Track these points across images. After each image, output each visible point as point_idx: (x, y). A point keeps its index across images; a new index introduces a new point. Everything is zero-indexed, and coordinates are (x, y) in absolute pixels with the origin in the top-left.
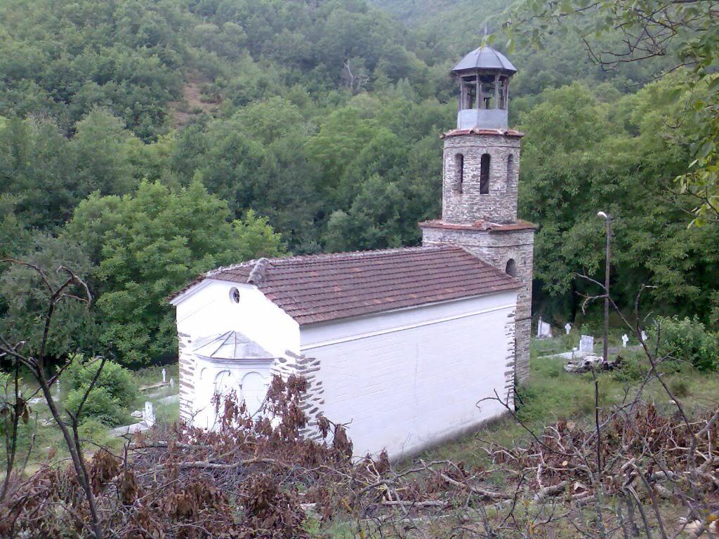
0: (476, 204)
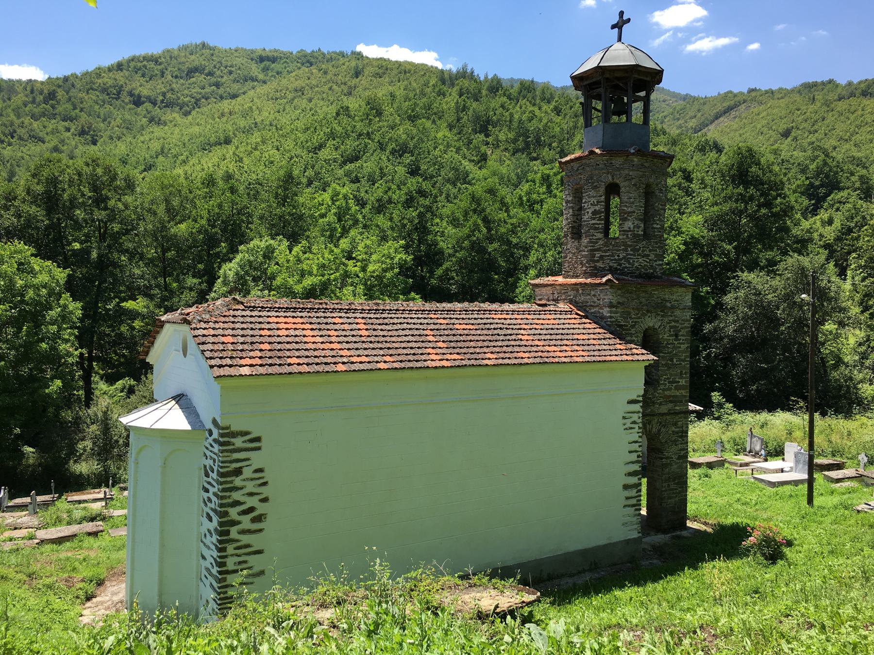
0: (598, 250)
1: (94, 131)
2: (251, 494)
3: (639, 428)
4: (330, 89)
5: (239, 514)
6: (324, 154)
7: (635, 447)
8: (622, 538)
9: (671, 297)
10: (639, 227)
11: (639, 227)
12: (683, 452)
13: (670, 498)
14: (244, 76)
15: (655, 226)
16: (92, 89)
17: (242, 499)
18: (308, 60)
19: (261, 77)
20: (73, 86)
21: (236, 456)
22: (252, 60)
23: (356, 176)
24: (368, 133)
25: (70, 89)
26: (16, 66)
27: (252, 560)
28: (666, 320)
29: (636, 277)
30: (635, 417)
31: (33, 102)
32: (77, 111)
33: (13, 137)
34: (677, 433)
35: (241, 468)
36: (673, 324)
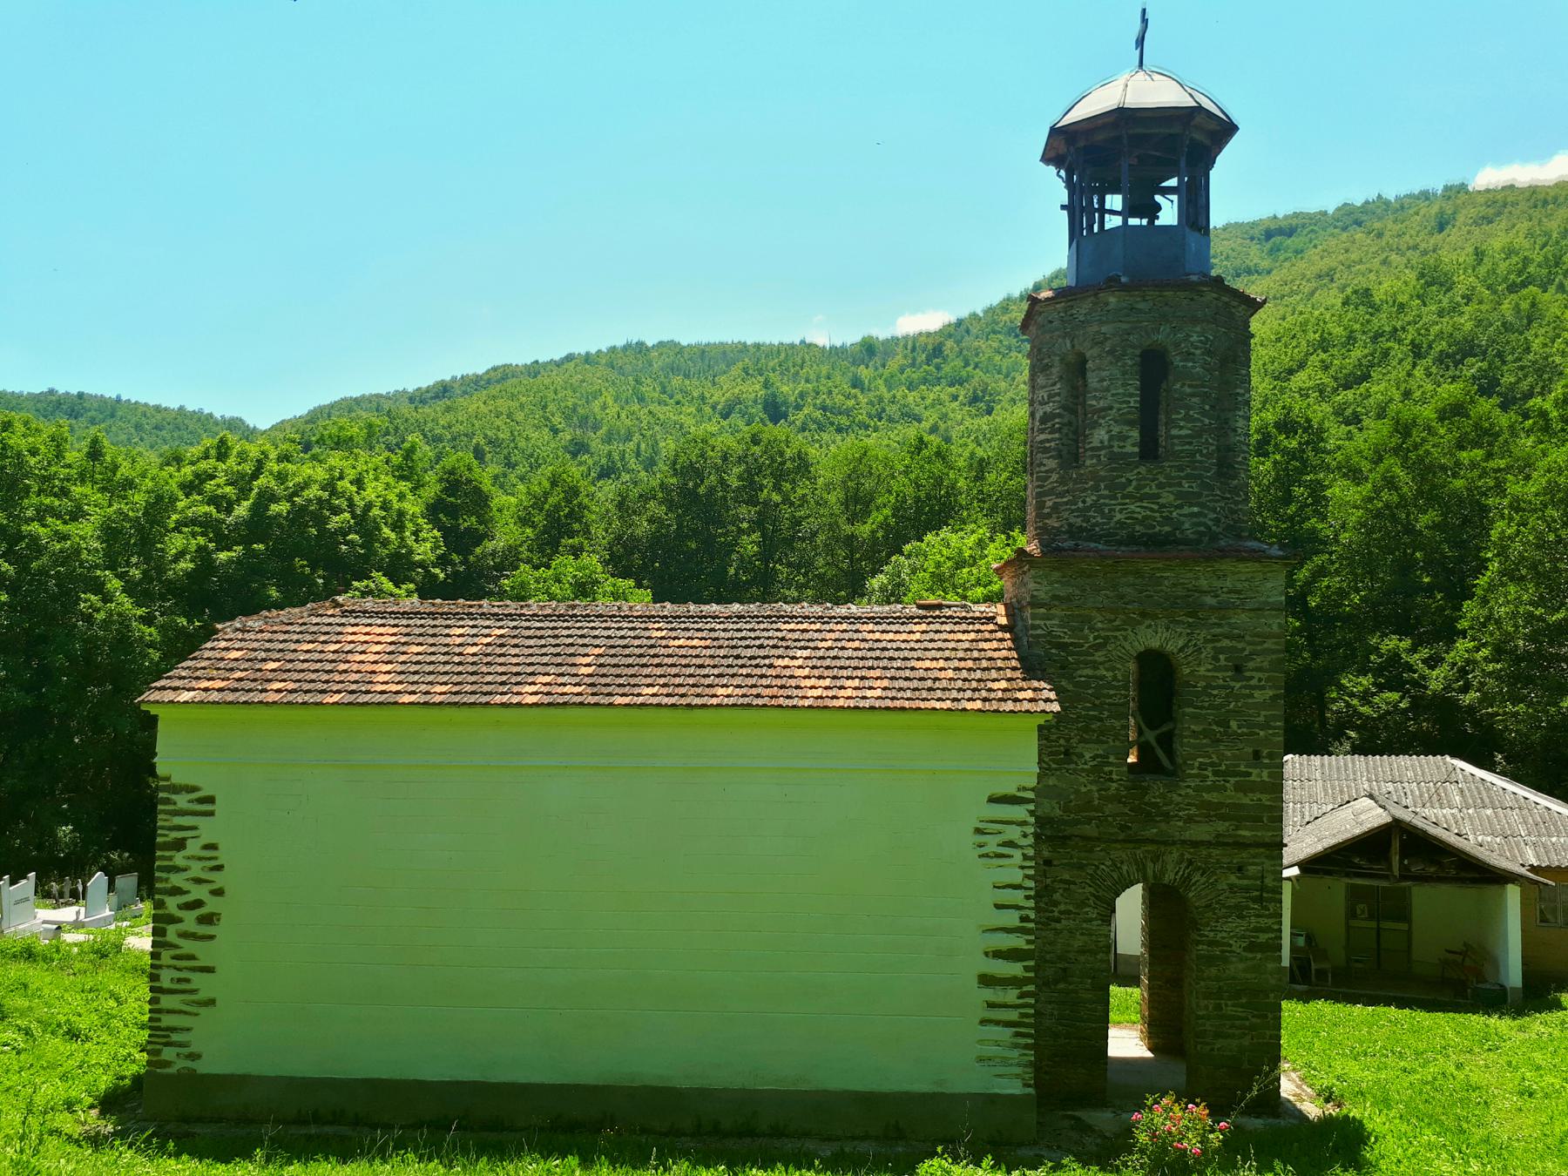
0: (1051, 492)
2: (198, 881)
4: (1385, 262)
5: (180, 907)
6: (1300, 379)
7: (1018, 897)
9: (1218, 584)
12: (1263, 937)
13: (1218, 1035)
15: (1174, 432)
16: (994, 332)
17: (185, 886)
18: (1351, 218)
19: (1265, 264)
20: (968, 331)
21: (178, 821)
22: (1252, 239)
23: (1355, 412)
24: (1396, 330)
27: (198, 980)
29: (1120, 543)
30: (1013, 833)
31: (913, 365)
34: (1247, 889)
35: (184, 839)
36: (1226, 643)
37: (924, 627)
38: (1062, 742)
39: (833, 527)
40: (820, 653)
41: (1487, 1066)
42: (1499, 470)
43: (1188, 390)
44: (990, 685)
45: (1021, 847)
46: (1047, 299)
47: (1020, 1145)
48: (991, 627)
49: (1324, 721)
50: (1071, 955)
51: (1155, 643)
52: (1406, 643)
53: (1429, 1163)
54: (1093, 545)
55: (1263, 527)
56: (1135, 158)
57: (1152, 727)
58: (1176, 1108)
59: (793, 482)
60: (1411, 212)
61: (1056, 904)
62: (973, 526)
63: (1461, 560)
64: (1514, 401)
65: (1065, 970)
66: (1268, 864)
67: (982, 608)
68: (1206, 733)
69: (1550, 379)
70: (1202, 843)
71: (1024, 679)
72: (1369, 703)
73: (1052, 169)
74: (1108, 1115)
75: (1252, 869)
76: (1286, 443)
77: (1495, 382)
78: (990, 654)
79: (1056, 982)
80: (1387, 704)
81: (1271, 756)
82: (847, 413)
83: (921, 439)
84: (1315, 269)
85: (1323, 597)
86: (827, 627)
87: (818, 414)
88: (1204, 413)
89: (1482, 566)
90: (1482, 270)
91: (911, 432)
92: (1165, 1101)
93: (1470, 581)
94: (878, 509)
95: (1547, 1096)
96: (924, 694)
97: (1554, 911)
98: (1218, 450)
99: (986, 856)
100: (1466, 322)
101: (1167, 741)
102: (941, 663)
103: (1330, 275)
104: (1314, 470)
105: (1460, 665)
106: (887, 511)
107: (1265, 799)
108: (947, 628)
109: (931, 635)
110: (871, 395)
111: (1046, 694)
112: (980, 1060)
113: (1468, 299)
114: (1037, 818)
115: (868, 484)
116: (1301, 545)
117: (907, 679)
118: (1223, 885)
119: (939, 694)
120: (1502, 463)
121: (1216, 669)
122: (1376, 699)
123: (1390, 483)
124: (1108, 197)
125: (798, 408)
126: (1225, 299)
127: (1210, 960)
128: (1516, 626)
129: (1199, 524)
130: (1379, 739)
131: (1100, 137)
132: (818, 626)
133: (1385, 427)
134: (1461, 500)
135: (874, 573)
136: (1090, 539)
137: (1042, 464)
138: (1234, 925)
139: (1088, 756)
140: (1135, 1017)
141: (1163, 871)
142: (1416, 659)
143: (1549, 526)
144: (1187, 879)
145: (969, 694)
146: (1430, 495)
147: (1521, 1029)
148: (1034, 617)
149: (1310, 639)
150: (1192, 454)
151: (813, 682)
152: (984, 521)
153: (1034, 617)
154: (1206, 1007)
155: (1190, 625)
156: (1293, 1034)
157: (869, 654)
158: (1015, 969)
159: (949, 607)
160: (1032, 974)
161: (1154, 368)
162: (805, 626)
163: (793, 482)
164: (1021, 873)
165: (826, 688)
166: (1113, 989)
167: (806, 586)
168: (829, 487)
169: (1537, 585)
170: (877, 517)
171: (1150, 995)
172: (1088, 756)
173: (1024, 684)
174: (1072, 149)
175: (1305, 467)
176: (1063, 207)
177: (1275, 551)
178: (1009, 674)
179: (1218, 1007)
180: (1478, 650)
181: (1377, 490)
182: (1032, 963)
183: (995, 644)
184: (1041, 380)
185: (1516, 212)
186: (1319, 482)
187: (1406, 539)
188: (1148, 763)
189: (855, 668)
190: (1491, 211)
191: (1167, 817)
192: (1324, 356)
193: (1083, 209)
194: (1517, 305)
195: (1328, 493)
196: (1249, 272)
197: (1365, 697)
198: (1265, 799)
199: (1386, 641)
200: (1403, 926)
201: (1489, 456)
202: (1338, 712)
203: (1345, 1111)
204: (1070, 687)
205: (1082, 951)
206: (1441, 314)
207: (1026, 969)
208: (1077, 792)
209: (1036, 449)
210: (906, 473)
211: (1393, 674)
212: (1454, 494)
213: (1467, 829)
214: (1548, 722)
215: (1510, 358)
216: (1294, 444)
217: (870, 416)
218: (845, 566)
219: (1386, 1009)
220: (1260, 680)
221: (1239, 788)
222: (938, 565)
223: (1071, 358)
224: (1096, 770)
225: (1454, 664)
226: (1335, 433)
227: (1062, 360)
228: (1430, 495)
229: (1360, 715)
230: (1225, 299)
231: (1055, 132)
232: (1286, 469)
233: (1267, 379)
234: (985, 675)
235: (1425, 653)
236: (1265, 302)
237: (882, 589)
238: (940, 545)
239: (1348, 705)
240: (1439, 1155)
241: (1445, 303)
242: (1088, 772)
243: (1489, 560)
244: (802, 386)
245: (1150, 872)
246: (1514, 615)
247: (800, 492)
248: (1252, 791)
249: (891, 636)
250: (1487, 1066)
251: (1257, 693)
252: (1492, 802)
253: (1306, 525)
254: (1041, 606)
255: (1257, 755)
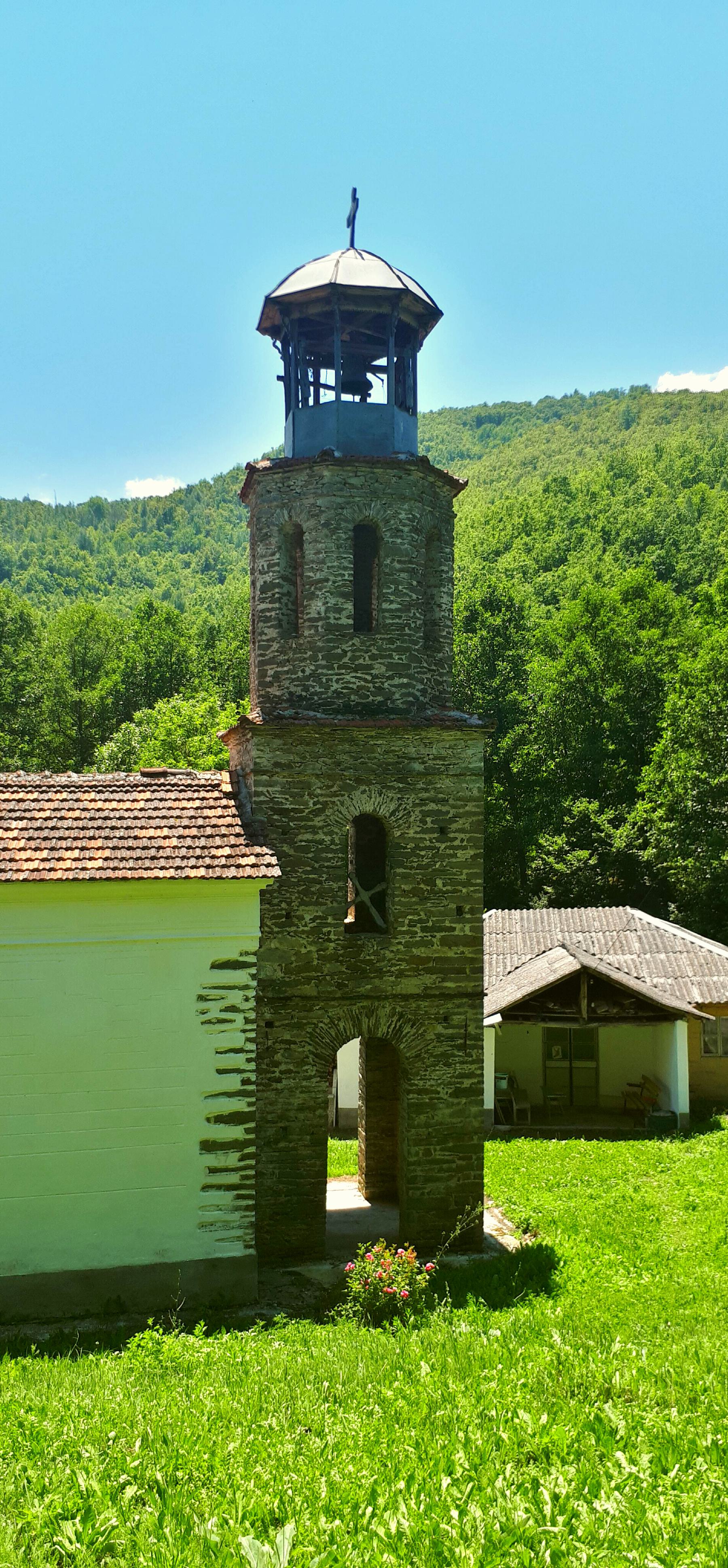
0: (272, 661)
1: (223, 564)
3: (247, 1021)
4: (580, 453)
6: (505, 561)
7: (239, 1060)
8: (198, 1254)
9: (424, 751)
10: (339, 610)
11: (339, 610)
12: (467, 1083)
13: (428, 1180)
14: (450, 453)
15: (385, 606)
16: (225, 501)
18: (552, 410)
19: (476, 449)
20: (198, 499)
22: (465, 424)
23: (553, 593)
24: (589, 517)
25: (193, 504)
26: (150, 480)
28: (411, 798)
29: (337, 712)
30: (235, 998)
31: (144, 529)
32: (201, 536)
33: (111, 583)
34: (452, 1038)
36: (432, 806)
37: (148, 795)
38: (284, 905)
39: (59, 692)
40: (38, 824)
41: (660, 1187)
42: (672, 648)
43: (397, 566)
44: (214, 852)
45: (243, 1011)
46: (265, 469)
47: (241, 1306)
48: (216, 794)
49: (524, 876)
50: (292, 1114)
51: (369, 808)
52: (595, 805)
53: (609, 1280)
54: (312, 713)
55: (470, 700)
56: (348, 334)
57: (367, 889)
58: (387, 1254)
59: (15, 644)
60: (604, 407)
61: (277, 1064)
62: (203, 694)
63: (641, 729)
64: (687, 585)
65: (285, 1129)
66: (470, 1013)
67: (208, 775)
68: (415, 892)
69: (716, 567)
70: (412, 996)
71: (247, 846)
72: (564, 861)
73: (268, 339)
74: (326, 1267)
75: (456, 1019)
76: (491, 620)
77: (671, 569)
78: (214, 821)
79: (277, 1142)
80: (579, 861)
81: (472, 911)
82: (76, 575)
83: (150, 605)
84: (520, 457)
85: (524, 764)
86: (45, 796)
87: (44, 575)
88: (411, 588)
89: (658, 735)
90: (661, 466)
91: (142, 596)
92: (376, 1249)
93: (647, 748)
94: (107, 674)
95: (707, 1209)
96: (147, 863)
97: (715, 1042)
98: (425, 624)
99: (209, 1022)
100: (647, 512)
101: (380, 901)
102: (166, 832)
103: (532, 463)
104: (515, 645)
105: (639, 825)
106: (117, 677)
107: (468, 952)
108: (172, 795)
109: (156, 804)
110: (101, 557)
111: (268, 859)
112: (202, 1226)
113: (649, 491)
114: (260, 981)
115: (97, 648)
116: (502, 717)
117: (129, 848)
118: (430, 1036)
119: (162, 862)
120: (673, 642)
121: (423, 831)
122: (569, 857)
123: (581, 658)
124: (323, 372)
125: (23, 567)
126: (431, 479)
127: (419, 1108)
128: (685, 788)
129: (409, 694)
130: (573, 893)
131: (313, 310)
132: (35, 795)
133: (577, 606)
134: (641, 675)
135: (103, 740)
136: (309, 708)
137: (262, 633)
138: (441, 1073)
139: (307, 917)
140: (354, 1169)
141: (377, 1025)
142: (602, 820)
143: (712, 699)
144: (398, 1031)
145: (193, 862)
146: (615, 670)
147: (688, 1150)
148: (257, 783)
149: (513, 802)
150: (402, 627)
151: (28, 854)
152: (216, 688)
153: (257, 783)
154: (417, 1154)
155: (400, 790)
156: (495, 1173)
157: (90, 824)
158: (236, 1132)
159: (174, 774)
160: (252, 1136)
161: (365, 542)
162: (21, 795)
163: (15, 644)
164: (243, 1036)
165: (43, 860)
166: (332, 1143)
167: (30, 754)
168: (53, 651)
169: (703, 752)
170: (105, 684)
171: (367, 1147)
172: (307, 917)
173: (247, 850)
174: (287, 320)
175: (508, 643)
176: (279, 378)
177: (475, 720)
178: (233, 840)
179: (427, 1153)
180: (654, 810)
181: (570, 666)
182: (252, 1125)
183: (219, 812)
184: (261, 549)
185: (690, 414)
186: (520, 657)
187: (594, 710)
188: (364, 923)
189: (75, 839)
190: (669, 412)
191: (380, 973)
192: (526, 539)
193: (298, 382)
194: (690, 499)
195: (528, 667)
196: (462, 456)
197: (560, 855)
198: (468, 952)
199: (578, 804)
200: (588, 1066)
201: (665, 635)
202: (537, 869)
203: (539, 1240)
204: (292, 852)
205: (301, 1109)
206: (627, 504)
207: (247, 1131)
208: (298, 953)
209: (258, 617)
210: (136, 639)
211: (583, 834)
212: (635, 669)
213: (644, 973)
214: (712, 873)
215: (683, 547)
216: (498, 621)
217: (100, 580)
218: (74, 733)
219: (577, 1142)
220: (462, 840)
221: (444, 942)
222: (169, 733)
223: (289, 529)
224: (315, 931)
225: (635, 824)
226: (536, 612)
227: (280, 531)
228: (615, 670)
229: (556, 872)
230: (431, 479)
231: (269, 301)
232: (491, 645)
233: (477, 560)
234: (210, 842)
235: (610, 814)
236: (466, 483)
237: (112, 757)
238: (169, 713)
239: (545, 863)
240: (617, 1271)
241: (630, 495)
242: (308, 933)
243: (664, 729)
244: (27, 545)
245: (365, 1027)
246: (683, 779)
247: (24, 655)
248: (456, 945)
249: (114, 805)
250: (660, 1187)
251: (460, 853)
252: (665, 947)
253: (510, 697)
254: (264, 773)
255: (460, 911)
